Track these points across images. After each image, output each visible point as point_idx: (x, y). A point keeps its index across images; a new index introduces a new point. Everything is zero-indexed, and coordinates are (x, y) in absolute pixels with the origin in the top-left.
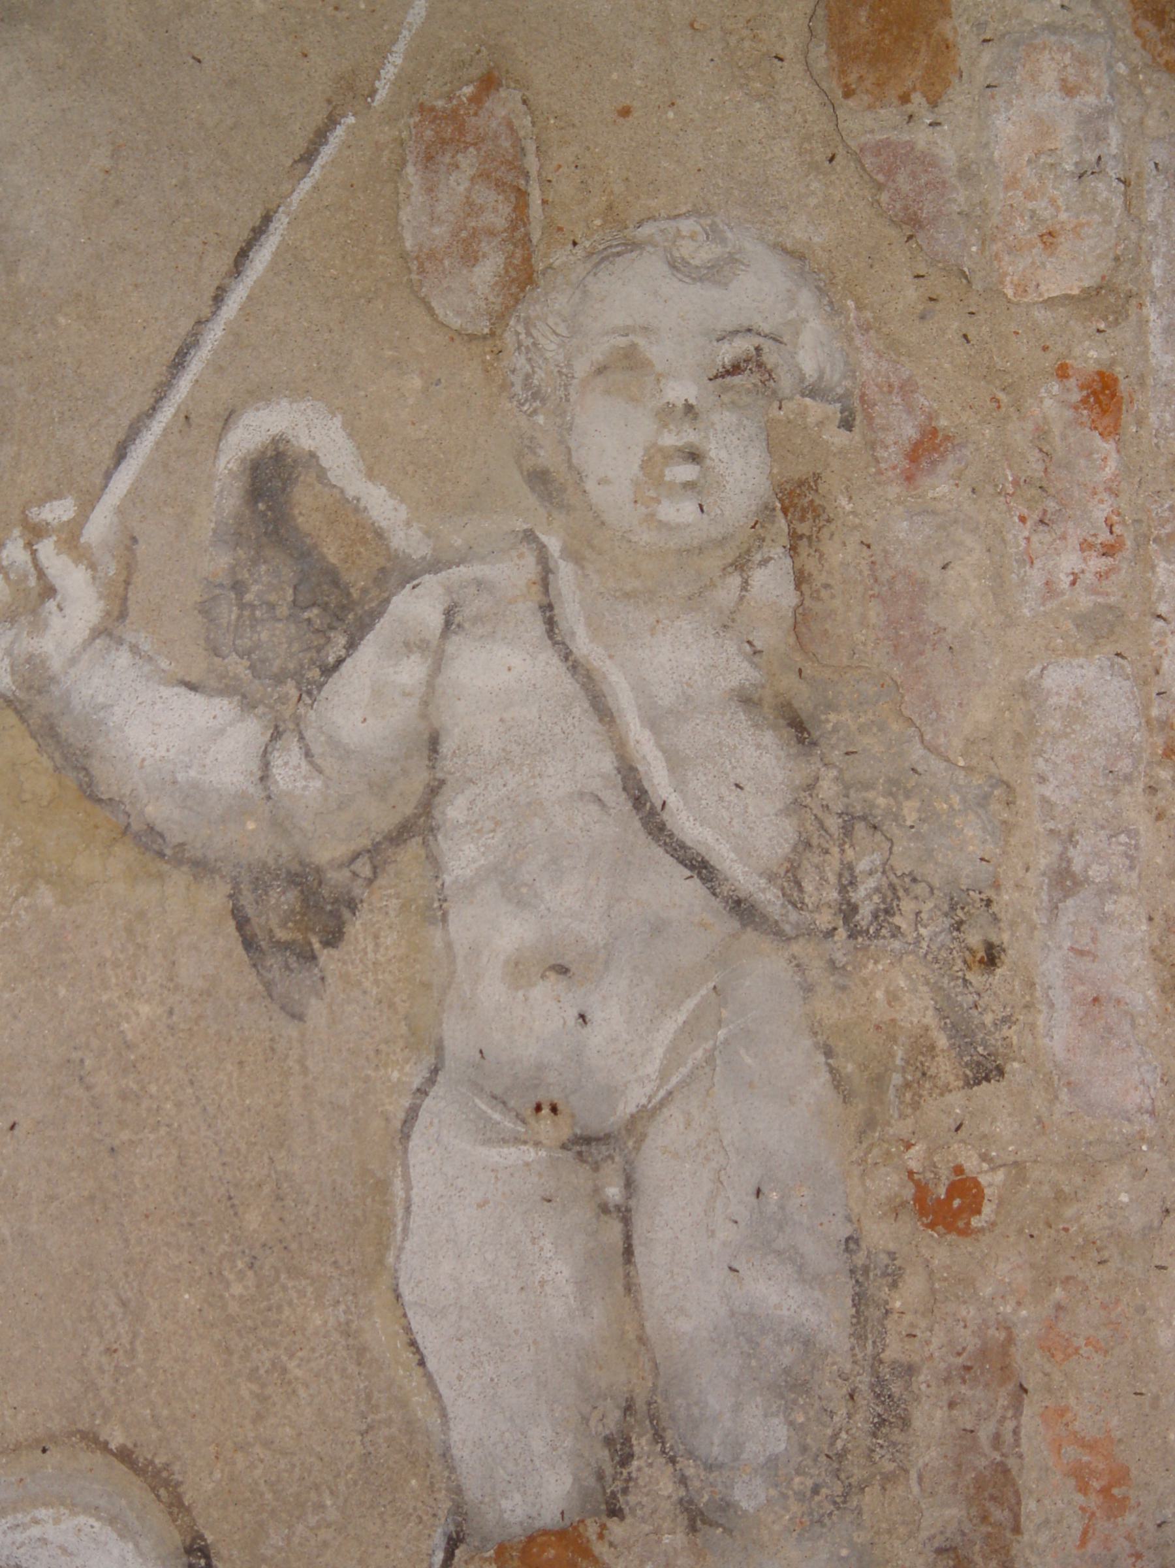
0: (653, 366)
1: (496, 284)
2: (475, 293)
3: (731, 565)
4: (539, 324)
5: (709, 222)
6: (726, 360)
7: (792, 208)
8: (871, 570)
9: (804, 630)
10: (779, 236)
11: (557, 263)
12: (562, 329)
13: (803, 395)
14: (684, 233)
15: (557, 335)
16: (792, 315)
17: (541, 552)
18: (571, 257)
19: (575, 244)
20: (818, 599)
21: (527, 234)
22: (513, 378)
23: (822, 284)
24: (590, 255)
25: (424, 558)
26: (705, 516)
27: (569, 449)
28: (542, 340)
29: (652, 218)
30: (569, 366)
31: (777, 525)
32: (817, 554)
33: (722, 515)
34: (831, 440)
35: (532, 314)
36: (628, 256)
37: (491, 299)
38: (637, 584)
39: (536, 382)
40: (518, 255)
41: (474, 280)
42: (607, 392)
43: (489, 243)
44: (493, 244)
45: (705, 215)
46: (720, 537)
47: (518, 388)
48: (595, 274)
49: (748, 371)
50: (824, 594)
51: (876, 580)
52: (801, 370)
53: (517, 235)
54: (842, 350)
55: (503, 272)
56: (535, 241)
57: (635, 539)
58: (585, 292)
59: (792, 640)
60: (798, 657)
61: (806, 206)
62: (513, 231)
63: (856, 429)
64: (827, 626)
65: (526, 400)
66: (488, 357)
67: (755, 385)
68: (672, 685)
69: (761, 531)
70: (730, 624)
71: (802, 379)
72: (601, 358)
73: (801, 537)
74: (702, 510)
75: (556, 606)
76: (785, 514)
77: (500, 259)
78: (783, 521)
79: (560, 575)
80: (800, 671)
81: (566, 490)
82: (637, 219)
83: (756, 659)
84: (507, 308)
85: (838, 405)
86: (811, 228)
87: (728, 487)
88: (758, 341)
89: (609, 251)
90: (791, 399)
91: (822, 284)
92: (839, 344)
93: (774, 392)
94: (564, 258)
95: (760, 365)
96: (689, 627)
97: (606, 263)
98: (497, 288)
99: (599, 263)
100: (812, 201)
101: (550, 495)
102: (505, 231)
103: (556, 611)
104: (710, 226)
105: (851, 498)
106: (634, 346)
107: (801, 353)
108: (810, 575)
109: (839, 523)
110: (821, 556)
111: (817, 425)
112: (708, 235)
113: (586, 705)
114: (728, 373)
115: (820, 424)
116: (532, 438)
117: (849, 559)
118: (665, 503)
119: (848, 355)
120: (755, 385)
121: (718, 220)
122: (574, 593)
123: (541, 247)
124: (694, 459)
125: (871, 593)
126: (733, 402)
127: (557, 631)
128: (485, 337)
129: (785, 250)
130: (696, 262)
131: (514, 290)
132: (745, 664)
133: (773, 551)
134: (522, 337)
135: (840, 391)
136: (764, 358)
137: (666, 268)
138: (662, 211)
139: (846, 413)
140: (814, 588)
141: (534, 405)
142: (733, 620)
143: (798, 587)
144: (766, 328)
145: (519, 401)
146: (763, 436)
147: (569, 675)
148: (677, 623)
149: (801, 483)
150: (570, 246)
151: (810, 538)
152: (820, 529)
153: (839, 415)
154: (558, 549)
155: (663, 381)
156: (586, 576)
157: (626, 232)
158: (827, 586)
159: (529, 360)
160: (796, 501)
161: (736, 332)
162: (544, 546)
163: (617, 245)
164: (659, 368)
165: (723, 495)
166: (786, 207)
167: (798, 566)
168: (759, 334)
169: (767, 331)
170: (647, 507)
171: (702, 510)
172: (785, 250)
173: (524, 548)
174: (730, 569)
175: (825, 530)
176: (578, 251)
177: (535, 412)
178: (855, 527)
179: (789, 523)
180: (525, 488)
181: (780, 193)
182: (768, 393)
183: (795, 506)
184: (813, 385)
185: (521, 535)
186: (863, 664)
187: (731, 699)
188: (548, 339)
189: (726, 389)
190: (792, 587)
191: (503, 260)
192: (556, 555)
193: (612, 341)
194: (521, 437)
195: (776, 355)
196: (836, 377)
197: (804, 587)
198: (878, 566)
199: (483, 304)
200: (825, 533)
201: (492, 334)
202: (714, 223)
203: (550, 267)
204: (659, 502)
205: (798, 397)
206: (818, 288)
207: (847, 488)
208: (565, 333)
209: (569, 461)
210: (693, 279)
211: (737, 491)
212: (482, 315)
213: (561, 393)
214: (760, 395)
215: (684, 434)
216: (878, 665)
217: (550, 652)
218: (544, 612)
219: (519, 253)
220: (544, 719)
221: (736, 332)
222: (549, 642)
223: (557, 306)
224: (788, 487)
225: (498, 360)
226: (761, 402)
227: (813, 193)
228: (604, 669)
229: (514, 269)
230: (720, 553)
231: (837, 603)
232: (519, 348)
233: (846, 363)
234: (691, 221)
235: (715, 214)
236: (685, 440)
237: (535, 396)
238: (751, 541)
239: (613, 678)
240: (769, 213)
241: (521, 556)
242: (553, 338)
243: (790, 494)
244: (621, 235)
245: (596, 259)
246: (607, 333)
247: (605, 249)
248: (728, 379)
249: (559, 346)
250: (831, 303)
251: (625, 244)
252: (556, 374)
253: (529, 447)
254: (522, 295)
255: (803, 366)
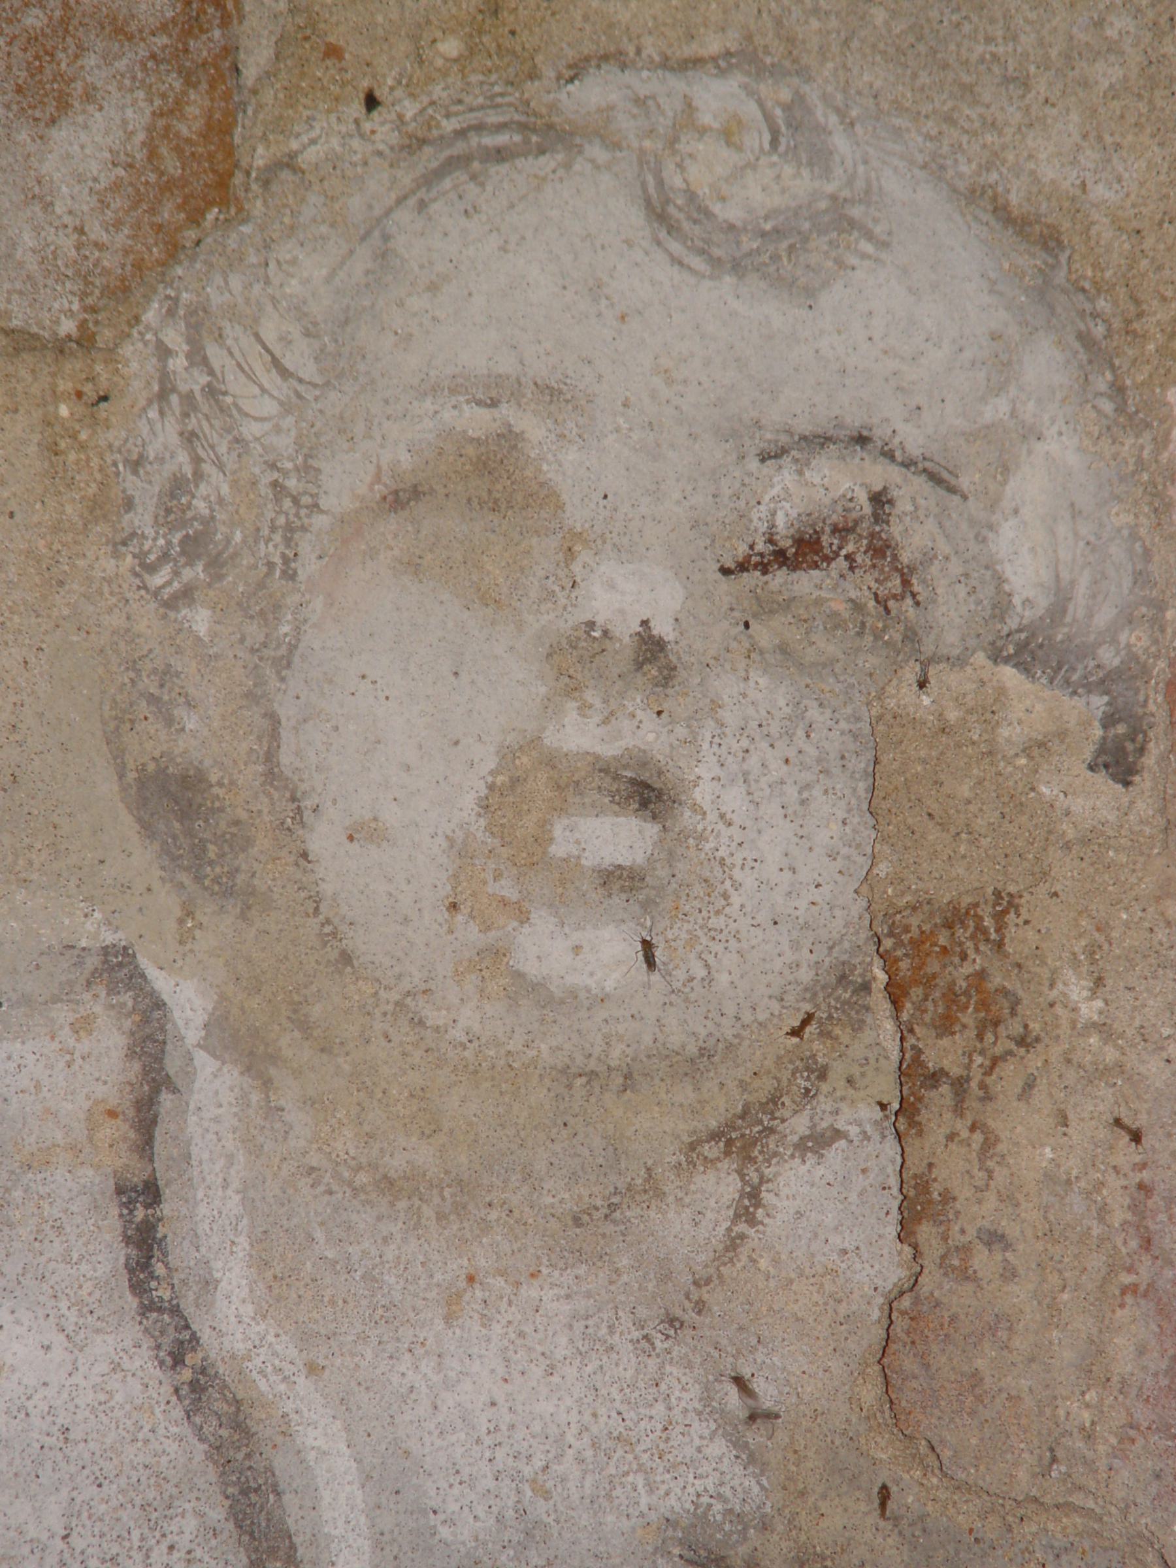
0: (561, 507)
1: (116, 186)
2: (48, 207)
3: (714, 1136)
4: (232, 332)
5: (785, 95)
6: (780, 521)
7: (1041, 87)
8: (1133, 1207)
9: (909, 1364)
10: (988, 167)
11: (311, 155)
12: (300, 359)
13: (997, 657)
14: (706, 119)
15: (284, 373)
16: (997, 410)
17: (146, 1021)
18: (356, 143)
19: (371, 102)
20: (965, 1275)
21: (229, 51)
22: (131, 483)
23: (1099, 330)
24: (414, 144)
25: (1080, 449)
26: (656, 977)
27: (274, 720)
28: (236, 384)
29: (617, 58)
30: (307, 470)
31: (868, 1036)
32: (978, 1137)
33: (708, 980)
34: (1062, 802)
35: (216, 298)
36: (529, 165)
37: (96, 232)
38: (425, 1155)
39: (200, 506)
40: (192, 110)
41: (50, 166)
42: (413, 566)
43: (107, 59)
44: (121, 65)
45: (776, 72)
46: (692, 1049)
47: (143, 519)
48: (422, 205)
49: (841, 563)
50: (983, 1261)
51: (1147, 1243)
52: (1000, 580)
53: (201, 48)
54: (1134, 536)
55: (140, 156)
56: (250, 74)
57: (435, 1017)
58: (383, 255)
59: (870, 1393)
60: (883, 1449)
61: (1085, 84)
62: (187, 33)
63: (1144, 782)
64: (980, 1363)
65: (165, 557)
66: (64, 411)
67: (857, 606)
68: (490, 1483)
69: (816, 1045)
70: (690, 1316)
71: (1001, 606)
72: (406, 460)
73: (935, 1078)
74: (650, 962)
75: (167, 1193)
76: (896, 1003)
77: (138, 115)
78: (889, 1026)
79: (195, 1100)
80: (884, 1494)
81: (249, 842)
82: (571, 54)
83: (755, 1437)
84: (138, 266)
85: (1099, 702)
86: (1090, 156)
87: (736, 900)
88: (879, 474)
89: (474, 140)
90: (959, 662)
91: (1099, 330)
92: (1127, 519)
93: (911, 636)
94: (335, 142)
95: (881, 549)
96: (565, 1308)
97: (461, 176)
98: (117, 203)
99: (439, 173)
100: (1106, 74)
101: (198, 851)
102: (164, 28)
103: (166, 1208)
104: (787, 108)
105: (1099, 982)
106: (510, 438)
107: (1008, 530)
108: (947, 1197)
109: (1055, 1052)
110: (989, 1144)
111: (1026, 751)
112: (774, 142)
113: (217, 1514)
114: (781, 557)
115: (1038, 748)
116: (166, 675)
117: (1073, 1165)
118: (542, 921)
119: (1147, 554)
120: (857, 606)
121: (812, 93)
122: (230, 1159)
123: (268, 96)
124: (644, 804)
125: (1127, 1279)
126: (784, 649)
127: (159, 1269)
128: (61, 348)
129: (1002, 211)
130: (731, 213)
131: (168, 213)
132: (718, 1447)
133: (847, 1112)
134: (178, 363)
135: (1109, 657)
136: (895, 530)
137: (636, 217)
138: (648, 41)
139: (1121, 729)
140: (956, 1238)
141: (187, 574)
142: (700, 1307)
143: (905, 1233)
144: (913, 440)
145: (141, 556)
146: (861, 764)
147: (178, 1413)
148: (530, 1291)
149: (955, 918)
150: (356, 108)
151: (960, 1085)
152: (995, 1061)
153: (1098, 732)
154: (200, 1018)
155: (584, 556)
156: (273, 1111)
157: (531, 88)
158: (994, 1239)
159: (190, 438)
160: (933, 966)
161: (820, 441)
162: (160, 1005)
163: (501, 127)
164: (577, 515)
165: (716, 922)
166: (1026, 84)
167: (916, 1165)
168: (890, 455)
169: (915, 451)
170: (486, 928)
171: (650, 962)
172: (1002, 211)
173: (96, 1004)
174: (711, 1150)
175: (1008, 1069)
176: (381, 125)
177: (187, 594)
178: (1103, 1072)
179: (905, 1032)
180: (127, 823)
181: (1012, 36)
182: (895, 634)
183: (929, 982)
184: (1032, 630)
185: (93, 962)
186: (1078, 1499)
187: (662, 1550)
188: (252, 378)
189: (767, 607)
190: (892, 1230)
191: (147, 118)
192: (192, 1036)
193: (447, 415)
194: (132, 665)
195: (931, 525)
196: (1104, 617)
197: (926, 1232)
198: (1155, 1201)
199: (67, 243)
200: (1010, 1076)
201: (85, 340)
202: (799, 99)
203: (289, 163)
204: (524, 918)
205: (980, 658)
206: (1085, 339)
207: (1092, 950)
208: (309, 371)
209: (270, 757)
210: (716, 262)
211: (763, 917)
212: (62, 278)
213: (274, 550)
214: (869, 639)
215: (627, 725)
216: (1125, 1513)
217: (132, 1332)
218: (129, 1205)
219: (197, 105)
220: (78, 1543)
221: (820, 441)
222: (132, 1302)
223: (294, 286)
224: (914, 921)
225: (94, 422)
226: (870, 661)
227: (1113, 48)
228: (289, 1406)
229: (178, 150)
230: (685, 1094)
231: (1019, 1294)
232: (162, 396)
233: (1140, 578)
234: (732, 84)
235: (804, 73)
236: (628, 742)
237: (193, 547)
238: (785, 1075)
239: (311, 1438)
240: (968, 90)
241: (81, 1027)
242: (271, 379)
243: (916, 944)
244: (514, 97)
245: (430, 159)
246: (435, 390)
247: (461, 133)
248: (779, 578)
249: (286, 408)
250: (1118, 390)
251: (523, 127)
252: (265, 490)
253: (153, 699)
254: (192, 234)
255: (1008, 571)
